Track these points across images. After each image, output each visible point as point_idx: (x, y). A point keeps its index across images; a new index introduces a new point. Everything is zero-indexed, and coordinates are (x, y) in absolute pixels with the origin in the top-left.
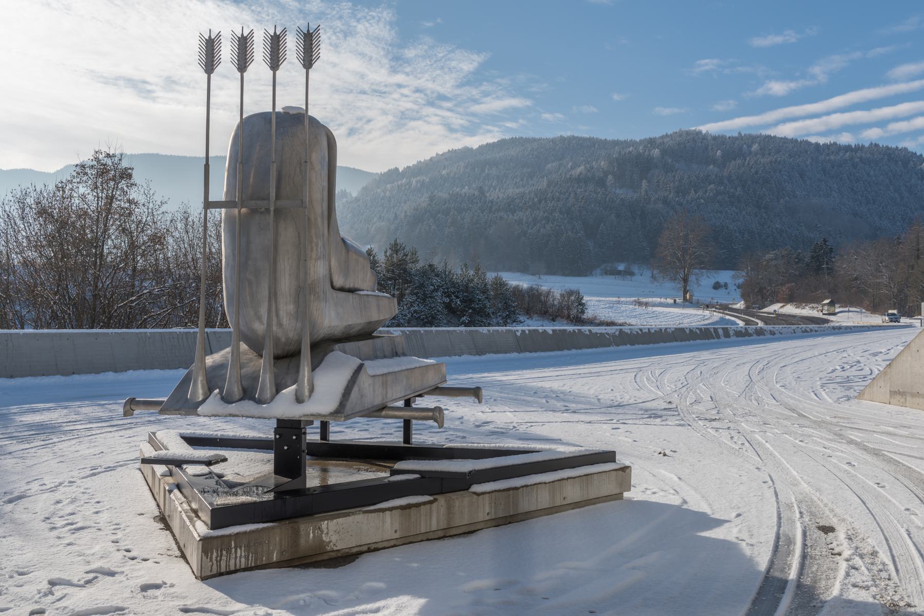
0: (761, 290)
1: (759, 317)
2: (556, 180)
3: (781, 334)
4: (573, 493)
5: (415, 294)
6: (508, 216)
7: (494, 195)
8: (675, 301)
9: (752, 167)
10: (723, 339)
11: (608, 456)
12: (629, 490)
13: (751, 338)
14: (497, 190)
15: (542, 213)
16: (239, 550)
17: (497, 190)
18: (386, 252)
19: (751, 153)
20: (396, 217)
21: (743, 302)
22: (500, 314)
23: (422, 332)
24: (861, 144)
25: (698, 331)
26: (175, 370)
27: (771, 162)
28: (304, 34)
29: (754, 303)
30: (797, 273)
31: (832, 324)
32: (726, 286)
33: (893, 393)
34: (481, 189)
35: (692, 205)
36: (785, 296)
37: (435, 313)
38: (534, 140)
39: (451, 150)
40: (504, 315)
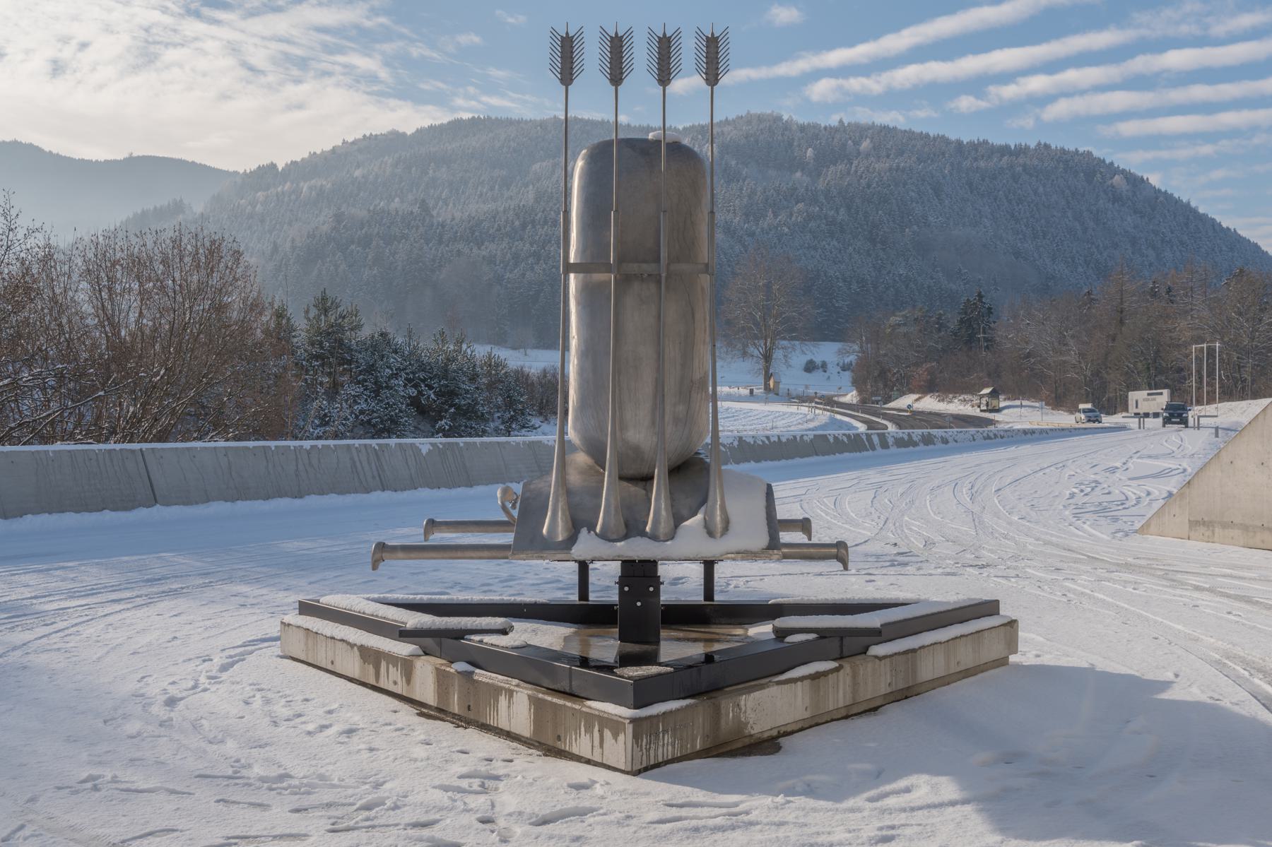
0: (883, 373)
1: (886, 417)
2: (550, 190)
3: (956, 441)
4: (966, 658)
5: (359, 382)
6: (471, 249)
7: (450, 212)
8: (752, 391)
9: (861, 177)
10: (879, 450)
11: (989, 608)
12: (1016, 652)
13: (917, 448)
14: (451, 205)
15: (527, 245)
16: (666, 736)
17: (451, 205)
18: (307, 312)
19: (859, 153)
20: (275, 249)
21: (854, 392)
22: (499, 414)
23: (462, 445)
24: (1023, 144)
25: (845, 439)
26: (98, 513)
27: (890, 169)
28: (707, 37)
29: (873, 394)
30: (940, 347)
31: (1000, 426)
32: (824, 366)
33: (1194, 524)
34: (423, 204)
35: (770, 235)
36: (922, 383)
37: (396, 414)
38: (510, 122)
39: (368, 135)
40: (507, 415)
